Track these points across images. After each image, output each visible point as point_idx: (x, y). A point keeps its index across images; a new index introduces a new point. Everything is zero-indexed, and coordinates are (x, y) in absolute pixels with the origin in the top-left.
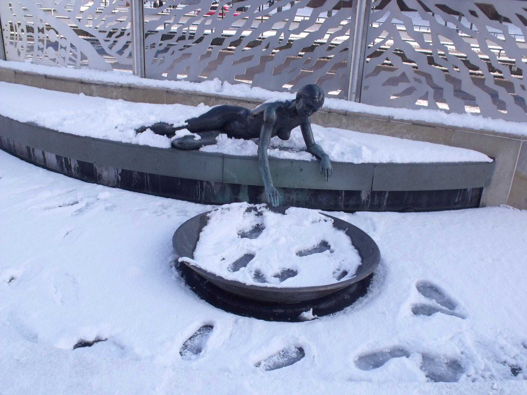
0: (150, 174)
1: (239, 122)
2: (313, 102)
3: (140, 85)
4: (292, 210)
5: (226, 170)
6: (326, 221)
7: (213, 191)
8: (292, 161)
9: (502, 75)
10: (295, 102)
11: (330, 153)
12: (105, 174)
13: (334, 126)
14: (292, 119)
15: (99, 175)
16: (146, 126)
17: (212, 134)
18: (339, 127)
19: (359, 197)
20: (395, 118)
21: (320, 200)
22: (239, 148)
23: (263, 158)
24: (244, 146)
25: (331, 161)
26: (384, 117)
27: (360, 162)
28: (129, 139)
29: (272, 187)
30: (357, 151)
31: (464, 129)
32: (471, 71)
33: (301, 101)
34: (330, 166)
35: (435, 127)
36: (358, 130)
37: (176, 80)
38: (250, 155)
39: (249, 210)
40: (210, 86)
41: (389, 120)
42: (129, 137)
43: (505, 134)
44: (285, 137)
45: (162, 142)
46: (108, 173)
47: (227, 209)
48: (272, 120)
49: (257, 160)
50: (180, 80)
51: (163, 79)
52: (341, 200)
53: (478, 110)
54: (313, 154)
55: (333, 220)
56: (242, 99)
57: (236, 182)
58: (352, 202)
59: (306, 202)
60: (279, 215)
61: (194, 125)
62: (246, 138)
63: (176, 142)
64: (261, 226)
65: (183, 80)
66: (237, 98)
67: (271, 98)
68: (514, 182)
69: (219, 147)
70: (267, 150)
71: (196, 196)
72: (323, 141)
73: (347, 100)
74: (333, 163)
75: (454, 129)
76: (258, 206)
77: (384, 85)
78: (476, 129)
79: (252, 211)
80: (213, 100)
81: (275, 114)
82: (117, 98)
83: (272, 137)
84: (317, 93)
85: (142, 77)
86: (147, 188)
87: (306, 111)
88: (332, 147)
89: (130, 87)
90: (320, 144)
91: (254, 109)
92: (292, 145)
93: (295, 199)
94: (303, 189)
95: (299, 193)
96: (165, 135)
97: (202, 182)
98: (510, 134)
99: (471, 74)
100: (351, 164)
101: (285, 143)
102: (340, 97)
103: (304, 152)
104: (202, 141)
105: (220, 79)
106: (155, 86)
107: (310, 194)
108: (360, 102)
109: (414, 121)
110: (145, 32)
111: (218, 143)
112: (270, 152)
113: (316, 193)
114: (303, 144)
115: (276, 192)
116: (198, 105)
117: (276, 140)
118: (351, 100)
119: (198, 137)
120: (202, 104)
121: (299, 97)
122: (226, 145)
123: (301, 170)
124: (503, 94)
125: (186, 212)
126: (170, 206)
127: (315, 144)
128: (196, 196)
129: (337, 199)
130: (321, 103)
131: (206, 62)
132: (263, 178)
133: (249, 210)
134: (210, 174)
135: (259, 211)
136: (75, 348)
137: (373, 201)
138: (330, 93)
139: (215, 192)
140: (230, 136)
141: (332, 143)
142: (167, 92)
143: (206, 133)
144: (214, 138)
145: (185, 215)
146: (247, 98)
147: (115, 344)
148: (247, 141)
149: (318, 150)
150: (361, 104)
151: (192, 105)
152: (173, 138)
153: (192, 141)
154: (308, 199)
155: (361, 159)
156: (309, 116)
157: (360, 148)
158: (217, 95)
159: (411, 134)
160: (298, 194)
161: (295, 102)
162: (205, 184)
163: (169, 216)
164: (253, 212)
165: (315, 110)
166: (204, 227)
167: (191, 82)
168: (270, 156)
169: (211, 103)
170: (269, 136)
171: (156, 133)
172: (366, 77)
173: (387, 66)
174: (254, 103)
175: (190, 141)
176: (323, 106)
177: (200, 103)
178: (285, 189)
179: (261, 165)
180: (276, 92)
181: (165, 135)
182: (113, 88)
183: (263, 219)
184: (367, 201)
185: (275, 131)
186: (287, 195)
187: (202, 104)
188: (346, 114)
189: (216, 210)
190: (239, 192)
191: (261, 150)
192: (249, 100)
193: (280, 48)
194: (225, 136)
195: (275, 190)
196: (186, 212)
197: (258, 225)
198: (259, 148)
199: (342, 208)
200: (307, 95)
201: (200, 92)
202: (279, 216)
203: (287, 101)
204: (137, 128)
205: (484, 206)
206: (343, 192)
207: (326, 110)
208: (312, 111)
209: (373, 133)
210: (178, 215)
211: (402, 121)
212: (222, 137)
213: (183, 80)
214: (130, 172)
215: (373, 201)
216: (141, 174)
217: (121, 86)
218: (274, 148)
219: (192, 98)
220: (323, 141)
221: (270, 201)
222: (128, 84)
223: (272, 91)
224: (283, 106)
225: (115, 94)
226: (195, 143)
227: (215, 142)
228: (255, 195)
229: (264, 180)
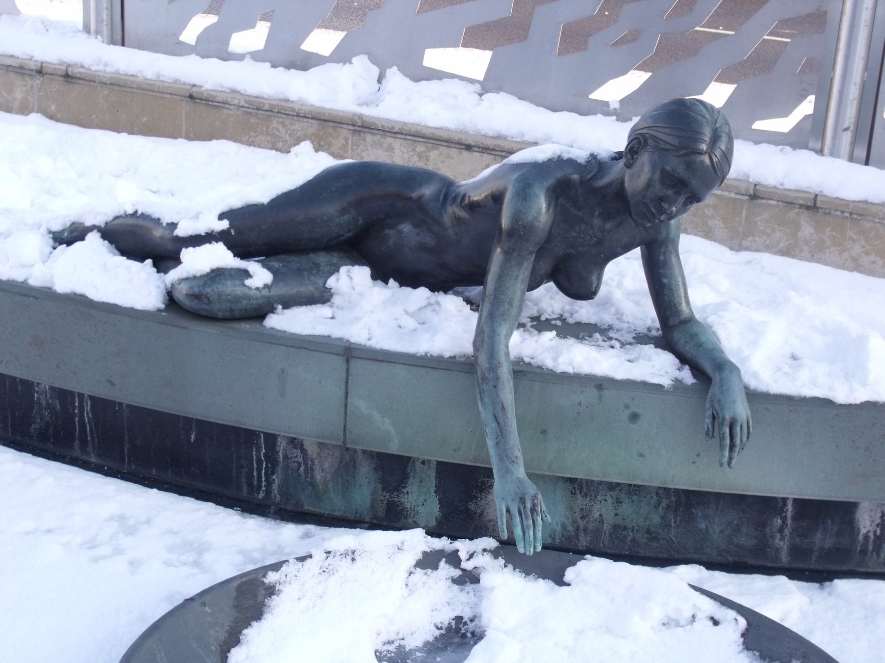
0: (92, 398)
1: (416, 225)
2: (690, 166)
3: (99, 68)
4: (591, 571)
5: (359, 403)
6: (716, 623)
7: (309, 471)
8: (601, 384)
10: (621, 163)
11: (746, 359)
13: (767, 248)
14: (608, 226)
16: (88, 223)
17: (317, 265)
18: (786, 252)
21: (702, 526)
22: (410, 323)
23: (494, 368)
24: (428, 314)
25: (746, 388)
27: (859, 396)
28: (23, 266)
29: (520, 482)
30: (848, 351)
33: (645, 159)
34: (741, 410)
36: (856, 266)
37: (227, 56)
38: (447, 355)
39: (429, 561)
40: (340, 86)
44: (579, 283)
45: (136, 287)
47: (345, 554)
48: (529, 229)
49: (470, 372)
50: (240, 57)
51: (178, 49)
52: (781, 530)
54: (683, 359)
55: (743, 623)
56: (445, 135)
57: (394, 448)
58: (822, 539)
59: (648, 532)
60: (543, 586)
61: (252, 232)
62: (440, 285)
63: (181, 294)
64: (471, 626)
65: (248, 60)
66: (427, 132)
67: (547, 139)
69: (339, 314)
70: (509, 335)
71: (250, 485)
72: (722, 306)
73: (820, 152)
74: (755, 397)
76: (463, 547)
79: (442, 564)
80: (345, 132)
81: (544, 206)
82: (24, 110)
83: (531, 288)
84: (707, 134)
85: (112, 42)
86: (84, 443)
87: (661, 199)
88: (755, 331)
89: (69, 76)
90: (711, 319)
91: (475, 177)
92: (607, 318)
93: (609, 518)
95: (623, 496)
96: (149, 262)
97: (271, 439)
100: (827, 403)
101: (584, 311)
102: (796, 140)
103: (649, 350)
104: (276, 292)
105: (373, 60)
106: (150, 74)
107: (665, 502)
108: (867, 163)
111: (336, 300)
112: (523, 345)
113: (687, 502)
114: (645, 314)
115: (535, 497)
116: (294, 150)
117: (549, 299)
118: (833, 154)
119: (260, 276)
120: (306, 146)
121: (638, 143)
122: (365, 309)
125: (202, 549)
126: (148, 522)
127: (691, 320)
128: (250, 485)
130: (718, 172)
132: (490, 443)
133: (429, 561)
134: (295, 411)
135: (468, 565)
138: (759, 125)
139: (319, 477)
140: (380, 275)
141: (758, 316)
142: (191, 97)
143: (295, 261)
144: (320, 282)
145: (196, 564)
148: (441, 297)
149: (700, 345)
150: (871, 171)
151: (274, 147)
152: (174, 274)
153: (239, 291)
154: (656, 519)
155: (864, 384)
156: (671, 217)
157: (861, 342)
158: (360, 116)
160: (619, 502)
161: (621, 163)
162: (282, 446)
163: (134, 564)
165: (695, 198)
166: (247, 625)
167: (274, 66)
168: (520, 361)
169: (338, 143)
170: (519, 286)
174: (485, 150)
175: (229, 288)
176: (733, 173)
177: (298, 142)
178: (572, 480)
179: (481, 392)
180: (565, 114)
181: (149, 262)
182: (12, 76)
183: (478, 595)
185: (545, 266)
186: (580, 501)
187: (306, 146)
188: (813, 205)
189: (302, 559)
190: (404, 479)
191: (486, 338)
192: (470, 142)
194: (361, 274)
195: (531, 489)
196: (202, 549)
197: (459, 619)
198: (479, 332)
199: (785, 558)
200: (668, 138)
202: (540, 589)
203: (593, 156)
204: (56, 228)
206: (790, 507)
207: (743, 186)
208: (682, 199)
210: (168, 564)
212: (352, 280)
213: (248, 60)
214: (28, 386)
216: (64, 396)
217: (40, 71)
218: (540, 324)
219: (275, 123)
220: (722, 306)
221: (511, 532)
222: (62, 63)
223: (554, 110)
224: (576, 177)
225: (18, 95)
226: (249, 298)
227: (323, 297)
228: (460, 504)
229: (492, 451)
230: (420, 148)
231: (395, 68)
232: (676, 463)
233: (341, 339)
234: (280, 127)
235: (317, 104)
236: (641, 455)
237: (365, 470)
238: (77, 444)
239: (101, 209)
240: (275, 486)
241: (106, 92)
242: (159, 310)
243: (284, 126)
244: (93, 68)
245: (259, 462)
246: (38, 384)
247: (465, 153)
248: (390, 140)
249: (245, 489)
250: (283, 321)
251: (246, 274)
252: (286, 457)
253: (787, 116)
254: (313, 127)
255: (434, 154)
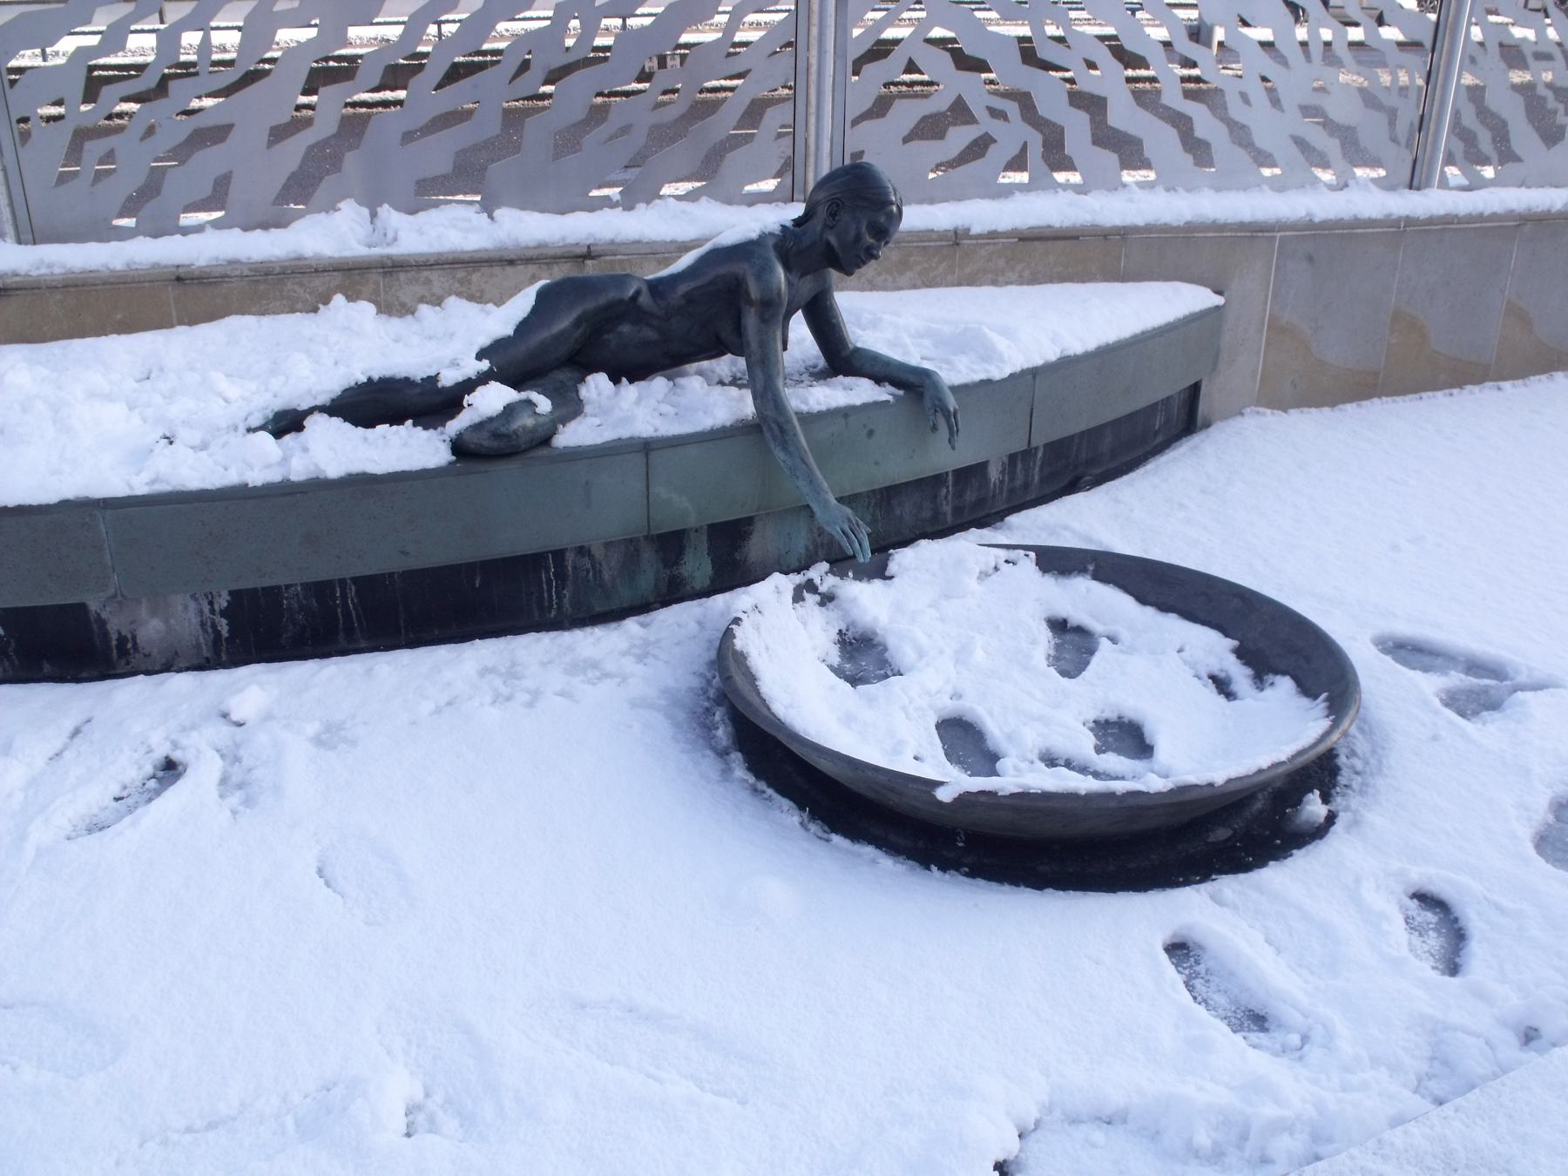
0: (355, 580)
3: (43, 271)
4: (902, 559)
5: (660, 491)
7: (598, 573)
9: (1195, 72)
12: (151, 630)
15: (122, 640)
16: (304, 406)
20: (976, 230)
26: (942, 235)
31: (1149, 228)
32: (1130, 73)
35: (1077, 238)
41: (957, 238)
42: (265, 462)
43: (1241, 226)
45: (411, 448)
46: (167, 622)
50: (199, 229)
53: (1152, 176)
55: (1032, 555)
56: (485, 256)
60: (877, 583)
61: (510, 362)
66: (466, 257)
68: (1268, 344)
74: (955, 389)
75: (1123, 234)
77: (906, 140)
78: (1175, 224)
79: (805, 594)
94: (855, 495)
97: (559, 555)
98: (1250, 223)
99: (1129, 80)
100: (988, 382)
106: (118, 265)
109: (1021, 232)
122: (615, 410)
124: (1205, 123)
129: (935, 497)
131: (294, 149)
134: (607, 517)
139: (606, 576)
142: (179, 279)
146: (500, 249)
147: (1075, 1121)
158: (389, 257)
159: (1019, 267)
162: (570, 558)
164: (812, 599)
171: (369, 423)
172: (855, 122)
173: (904, 88)
174: (528, 260)
184: (1002, 482)
192: (513, 256)
193: (226, 92)
201: (318, 257)
205: (1207, 425)
209: (915, 287)
211: (993, 235)
212: (597, 385)
214: (273, 593)
215: (1012, 479)
216: (320, 590)
223: (562, 213)
230: (461, 274)
231: (386, 206)
232: (901, 461)
233: (631, 438)
234: (296, 287)
235: (336, 255)
236: (877, 463)
237: (648, 556)
238: (341, 636)
239: (333, 381)
240: (566, 601)
241: (59, 297)
242: (450, 463)
243: (301, 285)
244: (34, 273)
245: (549, 582)
246: (288, 587)
247: (509, 269)
248: (426, 273)
249: (536, 614)
250: (572, 435)
251: (529, 403)
252: (575, 568)
254: (337, 278)
255: (475, 277)
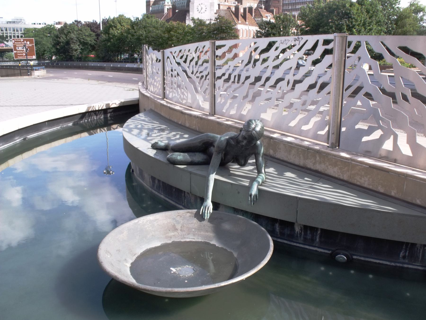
19: (293, 229)
110: (216, 77)
123: (239, 193)
136: (250, 76)
137: (306, 234)
159: (368, 176)
180: (292, 122)
184: (301, 234)
215: (306, 234)
236: (241, 202)
253: (308, 124)
